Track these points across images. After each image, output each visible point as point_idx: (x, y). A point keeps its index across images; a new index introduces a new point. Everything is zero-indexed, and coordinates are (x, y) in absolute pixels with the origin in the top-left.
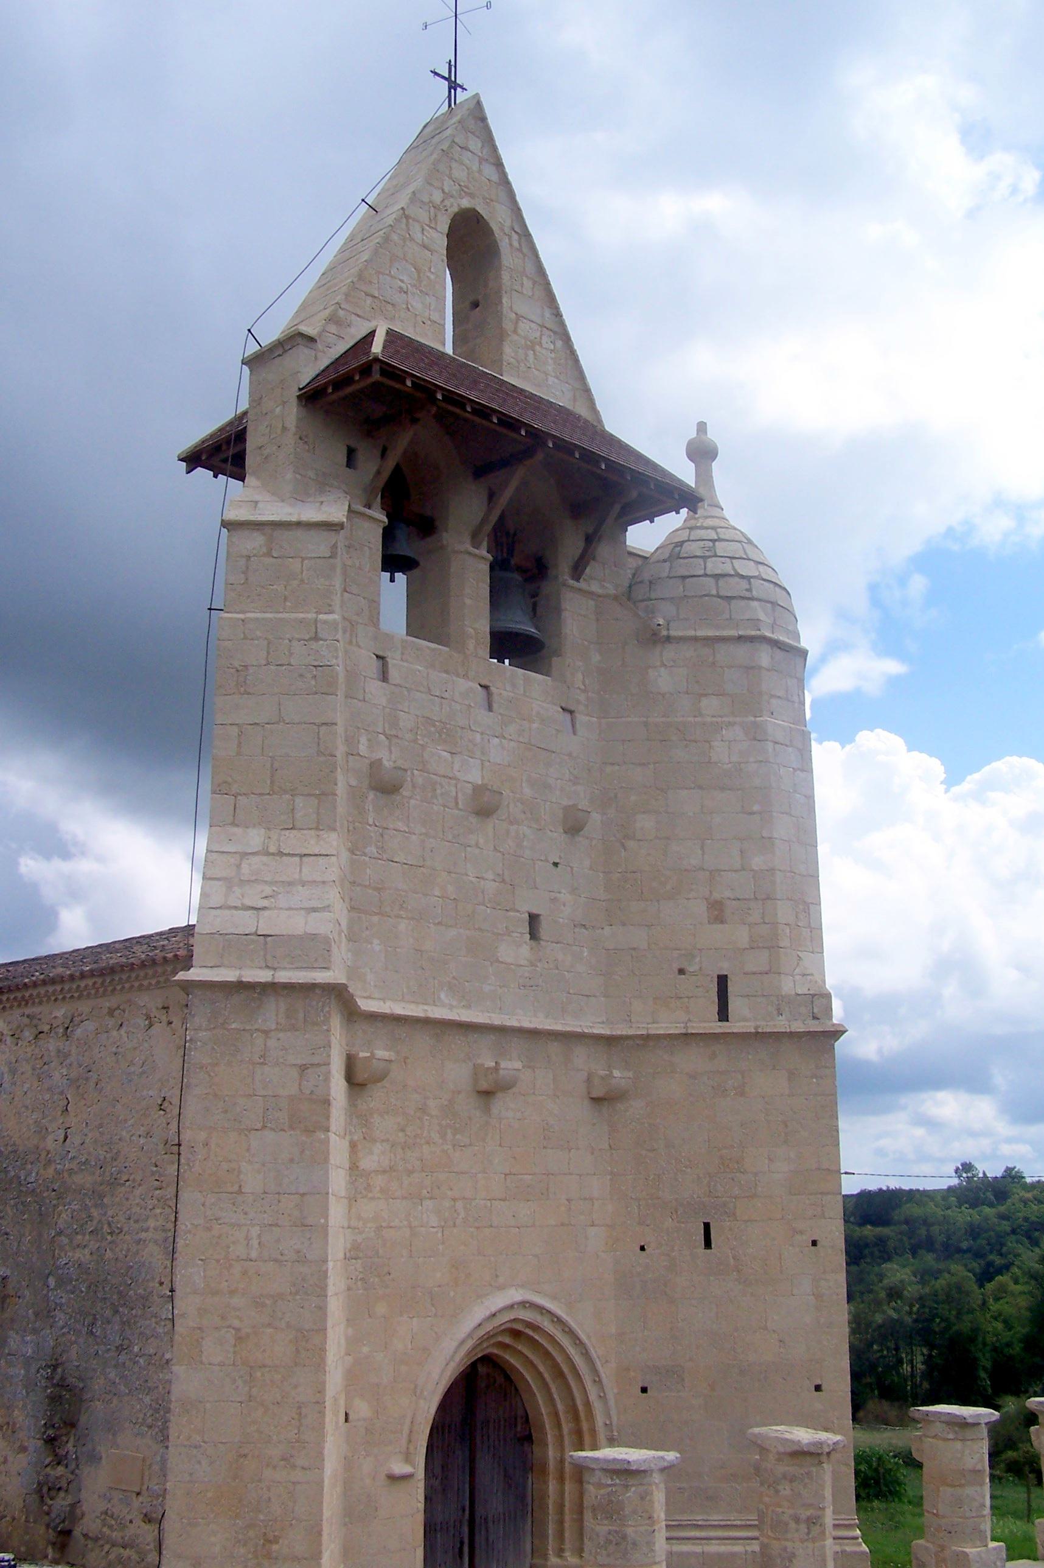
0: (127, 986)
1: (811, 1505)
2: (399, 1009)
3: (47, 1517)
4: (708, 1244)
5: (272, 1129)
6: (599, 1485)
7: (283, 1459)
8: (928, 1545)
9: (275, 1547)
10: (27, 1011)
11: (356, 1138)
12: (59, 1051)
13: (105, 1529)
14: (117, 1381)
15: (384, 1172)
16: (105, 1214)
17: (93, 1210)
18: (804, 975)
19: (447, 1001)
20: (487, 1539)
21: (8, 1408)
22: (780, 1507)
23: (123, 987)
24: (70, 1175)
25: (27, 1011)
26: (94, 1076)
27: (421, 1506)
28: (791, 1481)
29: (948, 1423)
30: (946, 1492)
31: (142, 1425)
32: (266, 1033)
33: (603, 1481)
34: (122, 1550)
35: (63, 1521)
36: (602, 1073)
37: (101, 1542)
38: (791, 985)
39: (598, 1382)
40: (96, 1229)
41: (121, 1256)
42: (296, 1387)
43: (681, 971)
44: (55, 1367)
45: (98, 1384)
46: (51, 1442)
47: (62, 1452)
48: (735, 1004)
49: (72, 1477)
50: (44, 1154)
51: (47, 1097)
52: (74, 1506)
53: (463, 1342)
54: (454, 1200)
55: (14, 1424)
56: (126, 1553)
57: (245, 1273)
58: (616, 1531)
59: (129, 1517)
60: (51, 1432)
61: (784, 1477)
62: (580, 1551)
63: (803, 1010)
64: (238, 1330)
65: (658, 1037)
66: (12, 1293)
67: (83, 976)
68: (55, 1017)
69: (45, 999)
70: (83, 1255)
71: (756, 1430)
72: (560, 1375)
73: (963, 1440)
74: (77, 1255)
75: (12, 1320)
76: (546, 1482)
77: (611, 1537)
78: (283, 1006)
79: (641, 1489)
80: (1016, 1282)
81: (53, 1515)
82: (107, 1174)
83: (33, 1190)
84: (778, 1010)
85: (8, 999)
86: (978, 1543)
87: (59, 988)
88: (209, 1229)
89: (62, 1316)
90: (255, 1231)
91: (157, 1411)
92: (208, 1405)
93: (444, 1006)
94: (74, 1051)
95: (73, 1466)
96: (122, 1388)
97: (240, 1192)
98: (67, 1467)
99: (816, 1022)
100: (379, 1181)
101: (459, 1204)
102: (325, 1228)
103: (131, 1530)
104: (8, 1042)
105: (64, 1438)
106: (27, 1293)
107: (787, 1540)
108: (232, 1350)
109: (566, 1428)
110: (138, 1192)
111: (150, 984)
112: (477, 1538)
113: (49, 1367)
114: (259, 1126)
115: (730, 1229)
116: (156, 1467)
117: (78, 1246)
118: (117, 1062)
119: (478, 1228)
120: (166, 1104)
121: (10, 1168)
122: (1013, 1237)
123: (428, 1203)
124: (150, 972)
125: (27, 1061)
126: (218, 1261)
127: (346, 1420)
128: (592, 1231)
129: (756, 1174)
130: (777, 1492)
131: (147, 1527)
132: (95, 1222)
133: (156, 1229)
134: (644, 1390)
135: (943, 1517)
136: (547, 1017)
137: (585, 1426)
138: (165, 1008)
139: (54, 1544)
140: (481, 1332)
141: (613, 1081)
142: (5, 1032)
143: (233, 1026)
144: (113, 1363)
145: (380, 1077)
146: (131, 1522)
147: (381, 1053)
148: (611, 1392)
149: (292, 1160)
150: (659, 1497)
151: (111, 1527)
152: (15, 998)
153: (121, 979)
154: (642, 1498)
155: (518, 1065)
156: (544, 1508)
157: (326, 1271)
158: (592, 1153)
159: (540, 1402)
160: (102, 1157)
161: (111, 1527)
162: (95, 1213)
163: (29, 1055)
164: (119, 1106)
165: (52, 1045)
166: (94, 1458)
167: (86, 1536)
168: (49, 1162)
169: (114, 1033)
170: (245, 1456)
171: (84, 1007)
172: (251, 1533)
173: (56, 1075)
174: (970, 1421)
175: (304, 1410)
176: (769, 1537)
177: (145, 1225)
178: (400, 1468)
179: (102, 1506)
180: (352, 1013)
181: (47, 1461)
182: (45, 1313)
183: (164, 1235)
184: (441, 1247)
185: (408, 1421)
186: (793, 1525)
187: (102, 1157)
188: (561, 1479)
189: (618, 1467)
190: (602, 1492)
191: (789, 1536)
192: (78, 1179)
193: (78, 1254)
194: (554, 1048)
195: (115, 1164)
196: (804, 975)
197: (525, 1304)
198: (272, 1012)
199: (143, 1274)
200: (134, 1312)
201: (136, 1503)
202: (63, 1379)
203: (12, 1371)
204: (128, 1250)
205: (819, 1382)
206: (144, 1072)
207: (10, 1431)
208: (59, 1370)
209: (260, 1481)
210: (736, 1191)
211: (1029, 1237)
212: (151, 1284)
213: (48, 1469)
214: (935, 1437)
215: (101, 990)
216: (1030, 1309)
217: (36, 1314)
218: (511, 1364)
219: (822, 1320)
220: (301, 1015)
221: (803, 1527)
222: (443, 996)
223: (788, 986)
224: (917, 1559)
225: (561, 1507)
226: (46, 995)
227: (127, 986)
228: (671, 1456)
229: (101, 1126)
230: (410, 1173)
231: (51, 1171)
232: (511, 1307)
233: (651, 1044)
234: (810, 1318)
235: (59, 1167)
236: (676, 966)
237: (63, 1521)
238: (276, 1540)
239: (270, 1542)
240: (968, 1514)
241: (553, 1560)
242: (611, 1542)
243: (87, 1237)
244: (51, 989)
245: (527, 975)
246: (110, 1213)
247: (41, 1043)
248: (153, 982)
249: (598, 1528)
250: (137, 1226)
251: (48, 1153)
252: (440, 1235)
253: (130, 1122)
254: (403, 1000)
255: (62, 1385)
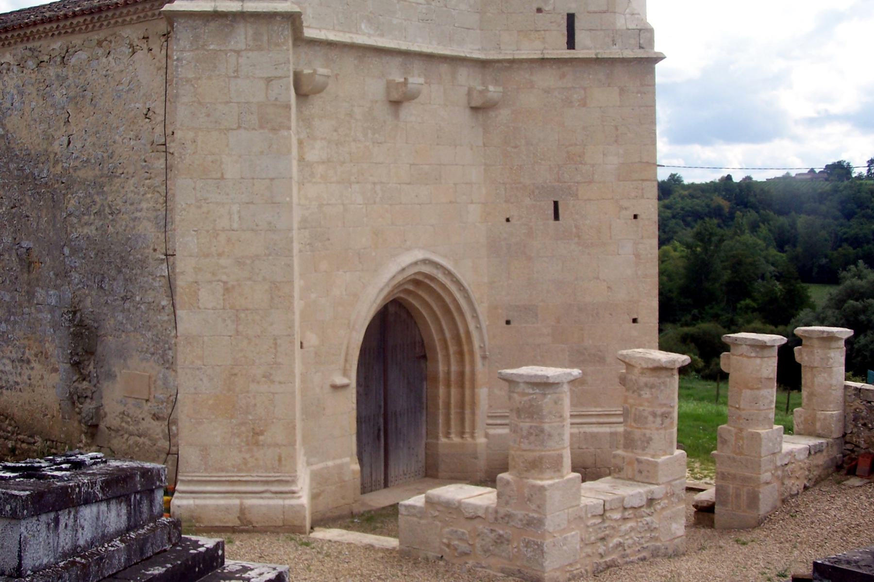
0: (113, 22)
1: (665, 405)
2: (332, 36)
3: (79, 416)
4: (556, 217)
5: (245, 128)
6: (524, 394)
7: (264, 377)
8: (730, 428)
9: (261, 438)
10: (29, 46)
11: (302, 137)
12: (58, 76)
13: (123, 424)
14: (124, 322)
15: (323, 162)
16: (106, 199)
17: (95, 196)
18: (633, 14)
19: (366, 31)
20: (396, 427)
21: (40, 342)
22: (641, 405)
23: (109, 23)
24: (75, 171)
25: (29, 46)
26: (89, 95)
27: (355, 406)
28: (651, 388)
29: (752, 346)
30: (747, 393)
31: (146, 352)
32: (238, 52)
33: (527, 391)
34: (138, 438)
35: (92, 419)
36: (480, 88)
37: (121, 433)
38: (623, 22)
39: (476, 317)
40: (99, 211)
41: (120, 230)
42: (272, 324)
43: (539, 10)
44: (75, 313)
45: (110, 324)
46: (77, 365)
47: (85, 372)
48: (579, 36)
49: (94, 389)
50: (52, 156)
51: (51, 112)
52: (98, 409)
53: (382, 290)
54: (374, 183)
55: (46, 353)
56: (141, 440)
57: (229, 240)
58: (536, 427)
59: (140, 416)
60: (76, 358)
61: (646, 385)
62: (462, 434)
63: (632, 41)
64: (225, 283)
65: (521, 61)
66: (36, 260)
67: (75, 15)
68: (53, 49)
69: (37, 37)
70: (90, 231)
71: (625, 352)
72: (447, 311)
73: (762, 358)
74: (85, 231)
75: (38, 280)
76: (437, 388)
77: (532, 431)
78: (250, 32)
79: (555, 396)
80: (675, 250)
81: (84, 415)
82: (106, 169)
83: (46, 183)
84: (613, 41)
85: (12, 36)
86: (767, 426)
87: (55, 25)
88: (200, 207)
89: (77, 276)
90: (235, 208)
91: (157, 343)
92: (206, 339)
93: (364, 34)
94: (70, 74)
95: (95, 381)
96: (129, 326)
97: (222, 178)
98: (90, 382)
99: (642, 50)
100: (320, 169)
101: (378, 187)
102: (290, 204)
103: (144, 425)
104: (15, 71)
105: (86, 363)
106: (47, 259)
107: (645, 428)
108: (221, 298)
109: (452, 349)
110: (132, 181)
111: (132, 19)
112: (390, 426)
113: (70, 312)
114: (235, 126)
115: (574, 206)
116: (160, 383)
117: (86, 224)
118: (107, 82)
119: (391, 205)
120: (150, 114)
121: (26, 167)
122: (674, 221)
123: (356, 187)
124: (132, 9)
125: (33, 85)
126: (208, 231)
127: (302, 347)
128: (471, 207)
129: (593, 166)
130: (640, 395)
131: (155, 423)
132: (98, 206)
133: (148, 210)
134: (508, 322)
135: (744, 410)
136: (439, 44)
137: (466, 348)
138: (146, 38)
139: (86, 433)
140: (395, 282)
141: (489, 95)
142: (12, 63)
143: (212, 47)
144: (120, 308)
145: (319, 90)
146: (143, 419)
147: (322, 71)
148: (485, 323)
149: (262, 153)
150: (567, 401)
151: (127, 423)
152: (19, 35)
153: (107, 16)
154: (556, 403)
155: (421, 80)
156: (436, 406)
157: (292, 237)
158: (472, 149)
159: (433, 331)
160: (100, 157)
161: (127, 423)
162: (97, 199)
163: (34, 80)
164: (111, 117)
165: (52, 71)
166: (111, 376)
167: (109, 428)
168: (56, 162)
169: (104, 60)
170: (236, 375)
171: (77, 40)
172: (243, 429)
173: (58, 95)
174: (769, 344)
175: (279, 342)
176: (631, 427)
177: (139, 207)
178: (340, 380)
179: (121, 408)
180: (299, 39)
181: (75, 378)
182: (64, 274)
183: (155, 214)
184: (365, 219)
185: (344, 347)
186: (651, 418)
187: (100, 157)
188: (448, 385)
189: (539, 381)
190: (526, 398)
191: (648, 426)
192: (81, 173)
193: (86, 230)
194: (444, 68)
195: (111, 161)
196: (633, 14)
197: (425, 261)
198: (242, 35)
199: (140, 244)
200: (134, 272)
201: (146, 407)
202: (81, 321)
203: (40, 316)
204: (127, 226)
205: (635, 316)
206: (130, 90)
207: (43, 358)
208: (78, 315)
209: (248, 392)
210: (579, 178)
211: (684, 221)
212: (147, 251)
213: (76, 384)
214: (741, 355)
215: (90, 26)
216: (685, 268)
217: (57, 275)
218: (411, 304)
219: (639, 273)
220: (265, 38)
221: (659, 420)
222: (363, 26)
223: (621, 23)
224: (721, 437)
225: (448, 405)
226: (44, 32)
227: (113, 22)
228: (576, 372)
229: (97, 132)
230: (342, 163)
231: (59, 168)
232: (416, 263)
233: (515, 66)
234: (630, 268)
235: (65, 165)
236: (535, 6)
237: (92, 419)
238: (261, 433)
239: (257, 434)
240: (762, 408)
241: (443, 440)
242: (532, 434)
243: (92, 217)
244: (48, 26)
245: (424, 11)
246: (110, 198)
247: (43, 70)
248: (135, 17)
249: (522, 424)
250: (132, 208)
251: (56, 154)
252: (364, 210)
253: (121, 129)
254: (334, 29)
255: (81, 324)
